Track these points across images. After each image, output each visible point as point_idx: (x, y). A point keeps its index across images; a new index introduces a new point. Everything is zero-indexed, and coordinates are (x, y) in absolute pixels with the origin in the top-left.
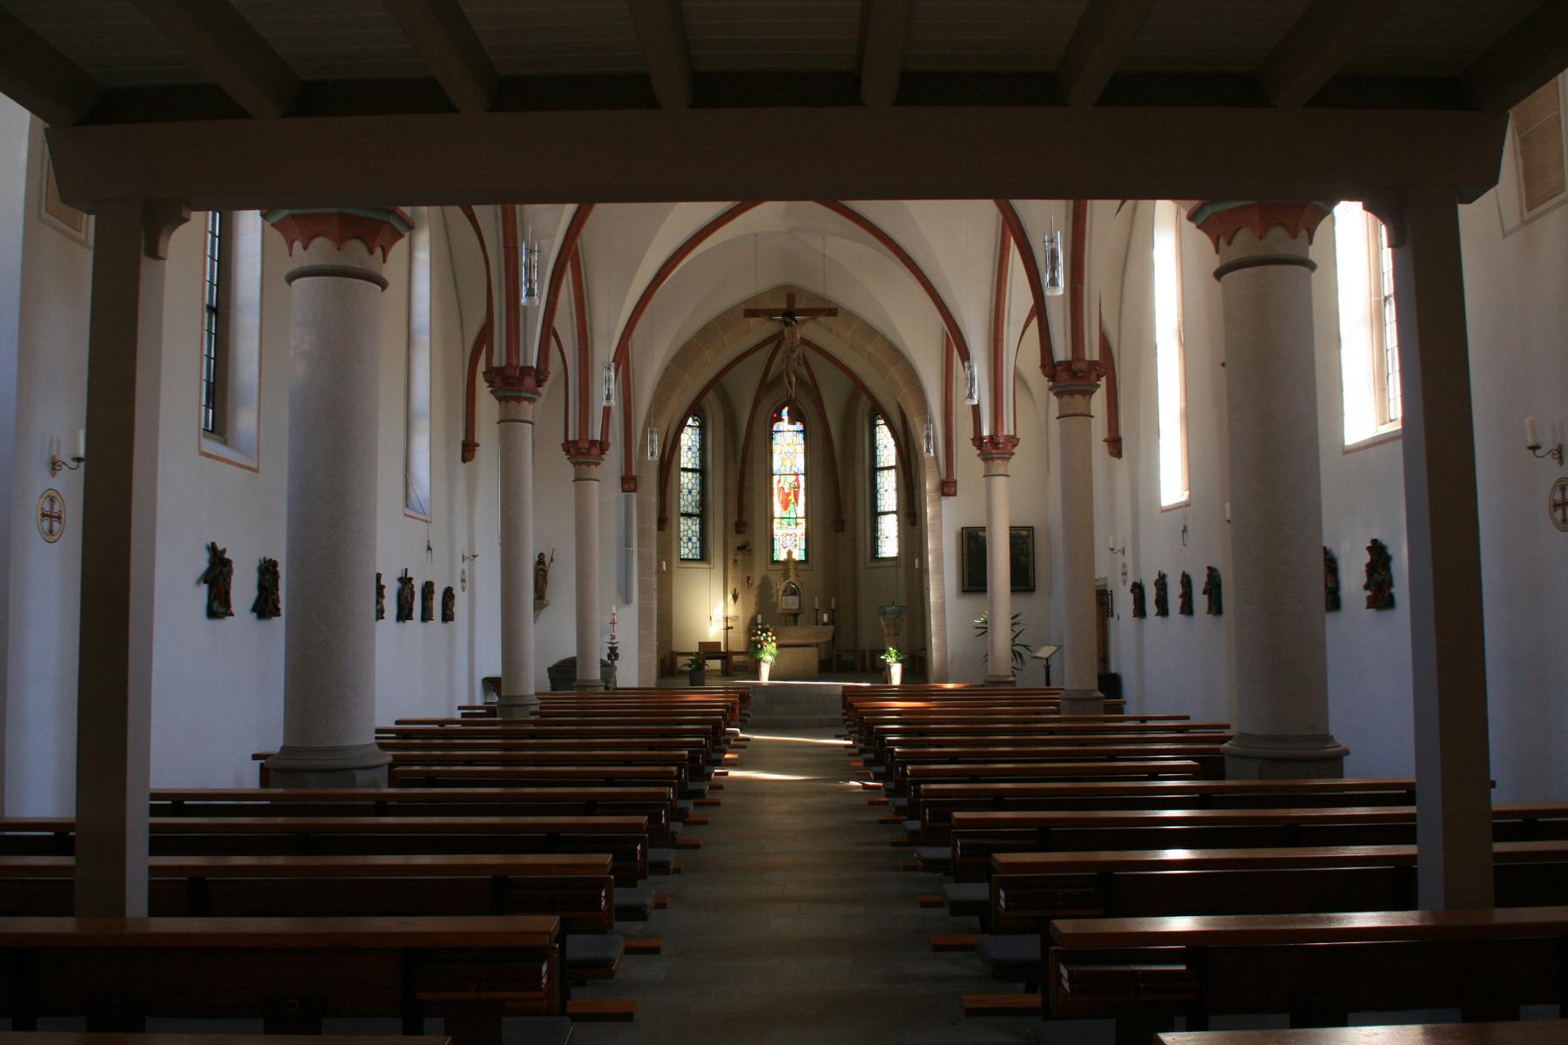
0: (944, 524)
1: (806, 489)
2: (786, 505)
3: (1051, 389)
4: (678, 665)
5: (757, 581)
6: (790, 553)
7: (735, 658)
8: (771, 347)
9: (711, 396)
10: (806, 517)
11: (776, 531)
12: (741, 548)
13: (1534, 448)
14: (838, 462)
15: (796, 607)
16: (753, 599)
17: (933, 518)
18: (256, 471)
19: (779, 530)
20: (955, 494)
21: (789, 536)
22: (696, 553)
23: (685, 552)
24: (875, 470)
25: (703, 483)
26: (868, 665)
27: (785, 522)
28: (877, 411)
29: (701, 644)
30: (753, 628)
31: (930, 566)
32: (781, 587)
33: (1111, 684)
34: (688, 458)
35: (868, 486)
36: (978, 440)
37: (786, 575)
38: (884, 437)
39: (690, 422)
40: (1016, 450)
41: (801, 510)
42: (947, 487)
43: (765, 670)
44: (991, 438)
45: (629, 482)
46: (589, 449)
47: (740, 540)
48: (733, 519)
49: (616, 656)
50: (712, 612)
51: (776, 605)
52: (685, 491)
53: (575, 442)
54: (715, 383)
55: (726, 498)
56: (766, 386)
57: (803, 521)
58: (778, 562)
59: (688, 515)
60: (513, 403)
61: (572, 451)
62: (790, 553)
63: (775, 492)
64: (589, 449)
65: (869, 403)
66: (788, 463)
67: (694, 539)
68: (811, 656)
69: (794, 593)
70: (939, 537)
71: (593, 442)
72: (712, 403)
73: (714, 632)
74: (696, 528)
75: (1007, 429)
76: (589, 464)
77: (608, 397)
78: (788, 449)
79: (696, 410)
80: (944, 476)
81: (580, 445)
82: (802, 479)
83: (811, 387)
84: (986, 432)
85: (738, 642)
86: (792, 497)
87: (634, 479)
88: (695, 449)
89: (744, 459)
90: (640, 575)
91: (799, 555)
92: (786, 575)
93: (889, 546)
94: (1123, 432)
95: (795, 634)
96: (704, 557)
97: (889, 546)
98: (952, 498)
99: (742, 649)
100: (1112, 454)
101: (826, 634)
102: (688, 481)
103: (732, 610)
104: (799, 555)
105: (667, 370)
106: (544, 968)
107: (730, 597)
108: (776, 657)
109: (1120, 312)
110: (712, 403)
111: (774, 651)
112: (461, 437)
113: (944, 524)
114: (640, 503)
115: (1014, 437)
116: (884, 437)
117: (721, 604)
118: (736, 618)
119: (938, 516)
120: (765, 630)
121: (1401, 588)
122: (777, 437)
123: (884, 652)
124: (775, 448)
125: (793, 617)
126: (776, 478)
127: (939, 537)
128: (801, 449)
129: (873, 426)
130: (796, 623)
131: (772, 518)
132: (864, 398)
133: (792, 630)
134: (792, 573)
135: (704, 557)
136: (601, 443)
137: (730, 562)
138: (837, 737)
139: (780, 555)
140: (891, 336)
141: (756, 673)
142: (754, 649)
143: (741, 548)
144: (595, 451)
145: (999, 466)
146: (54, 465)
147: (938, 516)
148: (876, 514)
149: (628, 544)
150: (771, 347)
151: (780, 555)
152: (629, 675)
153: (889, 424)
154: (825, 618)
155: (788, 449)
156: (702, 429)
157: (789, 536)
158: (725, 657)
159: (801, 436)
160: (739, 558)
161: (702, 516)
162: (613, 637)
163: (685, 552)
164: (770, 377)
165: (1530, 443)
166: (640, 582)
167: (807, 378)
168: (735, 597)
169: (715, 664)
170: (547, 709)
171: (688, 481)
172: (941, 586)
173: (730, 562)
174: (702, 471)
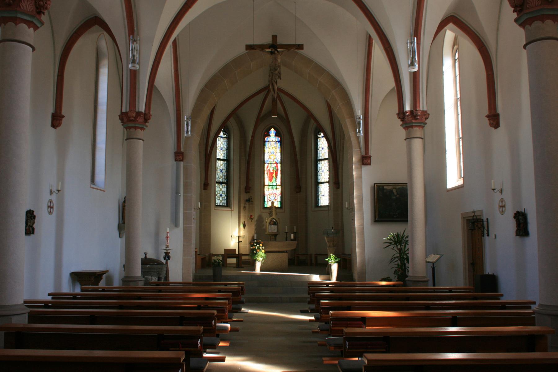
0: (363, 184)
1: (281, 171)
2: (271, 179)
3: (401, 125)
4: (211, 263)
5: (256, 217)
6: (273, 203)
7: (243, 258)
8: (262, 95)
9: (232, 120)
10: (281, 185)
11: (266, 192)
12: (248, 200)
13: (494, 190)
14: (298, 159)
15: (276, 231)
16: (253, 227)
17: (357, 178)
18: (104, 191)
19: (267, 191)
20: (370, 164)
21: (273, 195)
22: (224, 203)
23: (218, 202)
24: (317, 161)
25: (228, 167)
26: (313, 261)
27: (270, 187)
28: (319, 129)
29: (226, 250)
30: (252, 242)
31: (355, 206)
32: (268, 221)
33: (490, 283)
34: (220, 153)
35: (313, 167)
36: (402, 114)
37: (270, 214)
38: (323, 144)
39: (222, 134)
40: (427, 121)
41: (279, 181)
42: (365, 160)
43: (258, 266)
44: (411, 112)
45: (179, 156)
46: (136, 118)
47: (247, 196)
48: (243, 186)
49: (169, 258)
50: (232, 233)
51: (265, 230)
52: (219, 171)
53: (126, 113)
54: (234, 113)
55: (240, 175)
56: (259, 120)
57: (280, 187)
58: (267, 208)
59: (220, 183)
60: (11, 24)
61: (125, 120)
62: (273, 203)
63: (266, 172)
64: (136, 118)
65: (315, 124)
66: (272, 157)
67: (223, 195)
68: (284, 258)
69: (275, 224)
70: (360, 189)
71: (139, 113)
72: (232, 123)
73: (233, 244)
74: (225, 190)
75: (423, 106)
76: (136, 128)
77: (187, 132)
78: (272, 151)
79: (224, 127)
80: (363, 153)
81: (129, 114)
82: (279, 165)
83: (286, 120)
84: (408, 108)
85: (245, 249)
86: (274, 175)
87: (182, 153)
88: (224, 149)
89: (250, 154)
90: (184, 209)
91: (277, 204)
92: (270, 214)
93: (324, 200)
94: (500, 109)
95: (275, 245)
96: (228, 204)
97: (324, 200)
98: (368, 167)
99: (248, 253)
100: (491, 125)
101: (290, 246)
102: (220, 165)
103: (243, 232)
104: (277, 204)
105: (202, 91)
106: (199, 341)
107: (242, 226)
108: (265, 259)
109: (498, 30)
110: (232, 123)
111: (263, 255)
112: (51, 110)
113: (363, 184)
114: (185, 169)
115: (426, 112)
116: (323, 144)
117: (237, 229)
118: (244, 237)
119: (360, 177)
120: (258, 243)
121: (533, 226)
122: (267, 144)
123: (326, 256)
124: (266, 150)
125: (274, 236)
126: (266, 165)
127: (360, 189)
128: (279, 150)
129: (316, 138)
130: (275, 239)
131: (264, 185)
132: (312, 121)
133: (273, 243)
134: (274, 213)
135: (228, 204)
136: (145, 114)
137: (242, 208)
138: (303, 312)
139: (268, 204)
140: (333, 72)
141: (254, 269)
142: (253, 253)
143: (248, 200)
144: (140, 120)
145: (417, 132)
146: (51, 192)
147: (360, 177)
148: (317, 183)
149: (177, 191)
150: (262, 95)
151: (268, 204)
152: (178, 271)
153: (326, 136)
154: (292, 236)
155: (272, 151)
156: (228, 139)
157: (273, 195)
158: (238, 257)
159: (279, 144)
160: (247, 206)
161: (228, 184)
162: (167, 246)
163: (218, 202)
164: (262, 114)
165: (493, 187)
166: (184, 213)
167: (283, 113)
168: (244, 226)
169: (233, 261)
170: (120, 290)
171: (220, 165)
172: (362, 218)
173: (242, 208)
174: (228, 160)
